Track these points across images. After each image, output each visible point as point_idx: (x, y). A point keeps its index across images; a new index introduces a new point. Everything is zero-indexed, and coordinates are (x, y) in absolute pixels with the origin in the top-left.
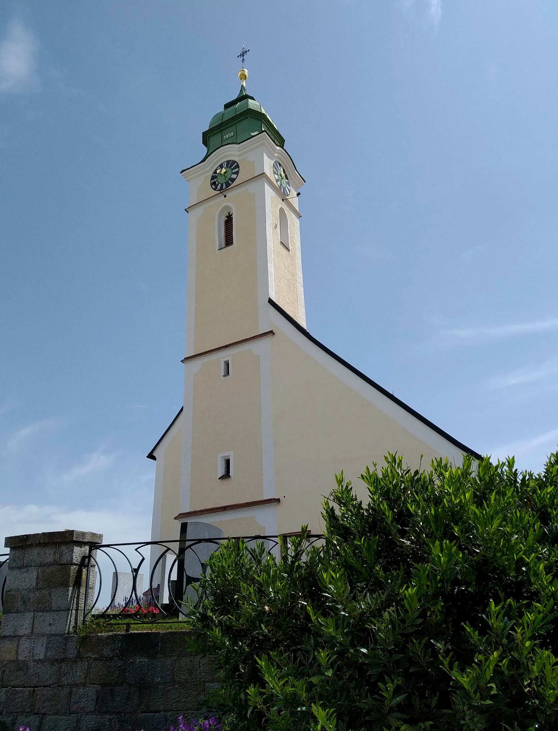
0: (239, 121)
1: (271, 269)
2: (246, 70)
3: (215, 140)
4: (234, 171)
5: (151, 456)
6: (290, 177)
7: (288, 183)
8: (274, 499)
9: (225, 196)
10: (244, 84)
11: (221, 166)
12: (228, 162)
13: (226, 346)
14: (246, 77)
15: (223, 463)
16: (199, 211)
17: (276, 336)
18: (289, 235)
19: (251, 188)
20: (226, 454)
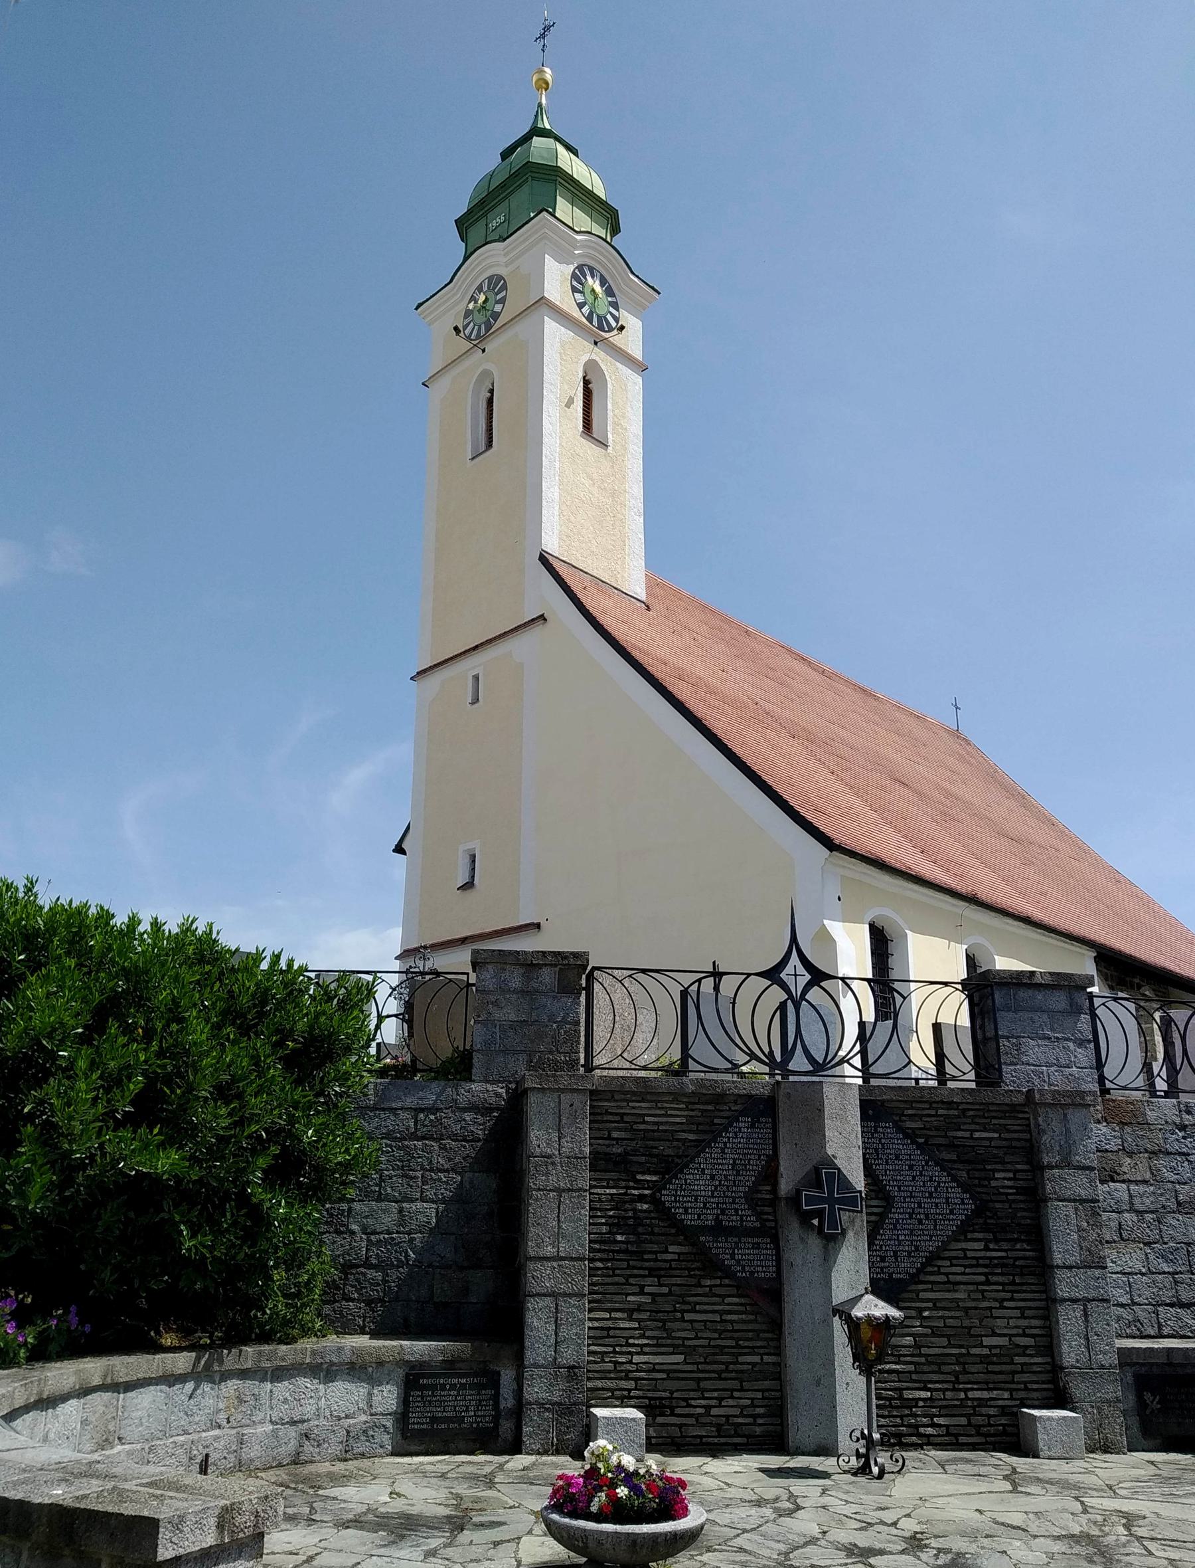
0: (517, 190)
1: (551, 491)
2: (547, 70)
3: (477, 233)
4: (498, 297)
5: (399, 849)
6: (619, 290)
7: (615, 305)
8: (533, 924)
9: (484, 351)
10: (544, 101)
11: (480, 289)
12: (490, 278)
13: (489, 641)
14: (547, 84)
15: (468, 860)
16: (445, 382)
17: (548, 624)
18: (610, 414)
19: (521, 329)
20: (470, 846)
